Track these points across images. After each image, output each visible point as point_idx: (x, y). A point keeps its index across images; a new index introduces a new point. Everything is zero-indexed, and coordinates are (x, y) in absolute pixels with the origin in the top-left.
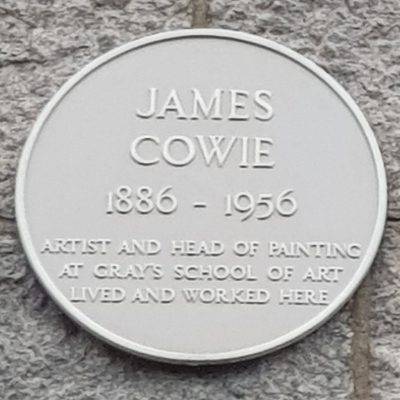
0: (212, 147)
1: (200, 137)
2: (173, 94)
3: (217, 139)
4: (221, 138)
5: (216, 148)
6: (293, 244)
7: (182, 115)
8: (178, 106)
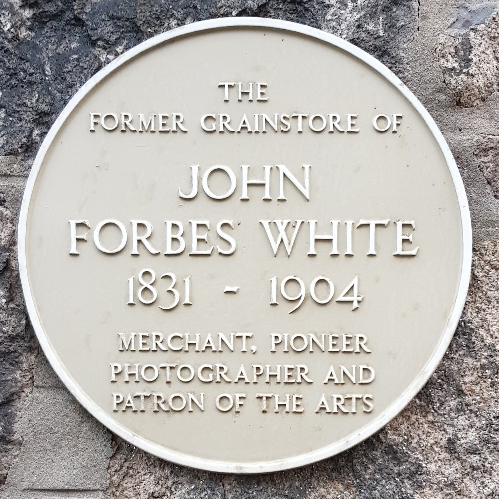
0: (279, 232)
1: (265, 223)
3: (282, 223)
4: (286, 222)
5: (283, 234)
6: (354, 366)
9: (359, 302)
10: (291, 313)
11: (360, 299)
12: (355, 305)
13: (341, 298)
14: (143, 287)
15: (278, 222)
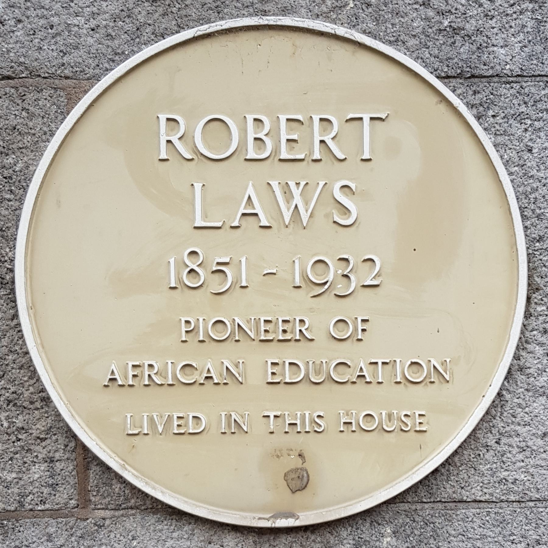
2: (250, 191)
5: (298, 200)
7: (264, 223)
8: (258, 210)
14: (188, 269)
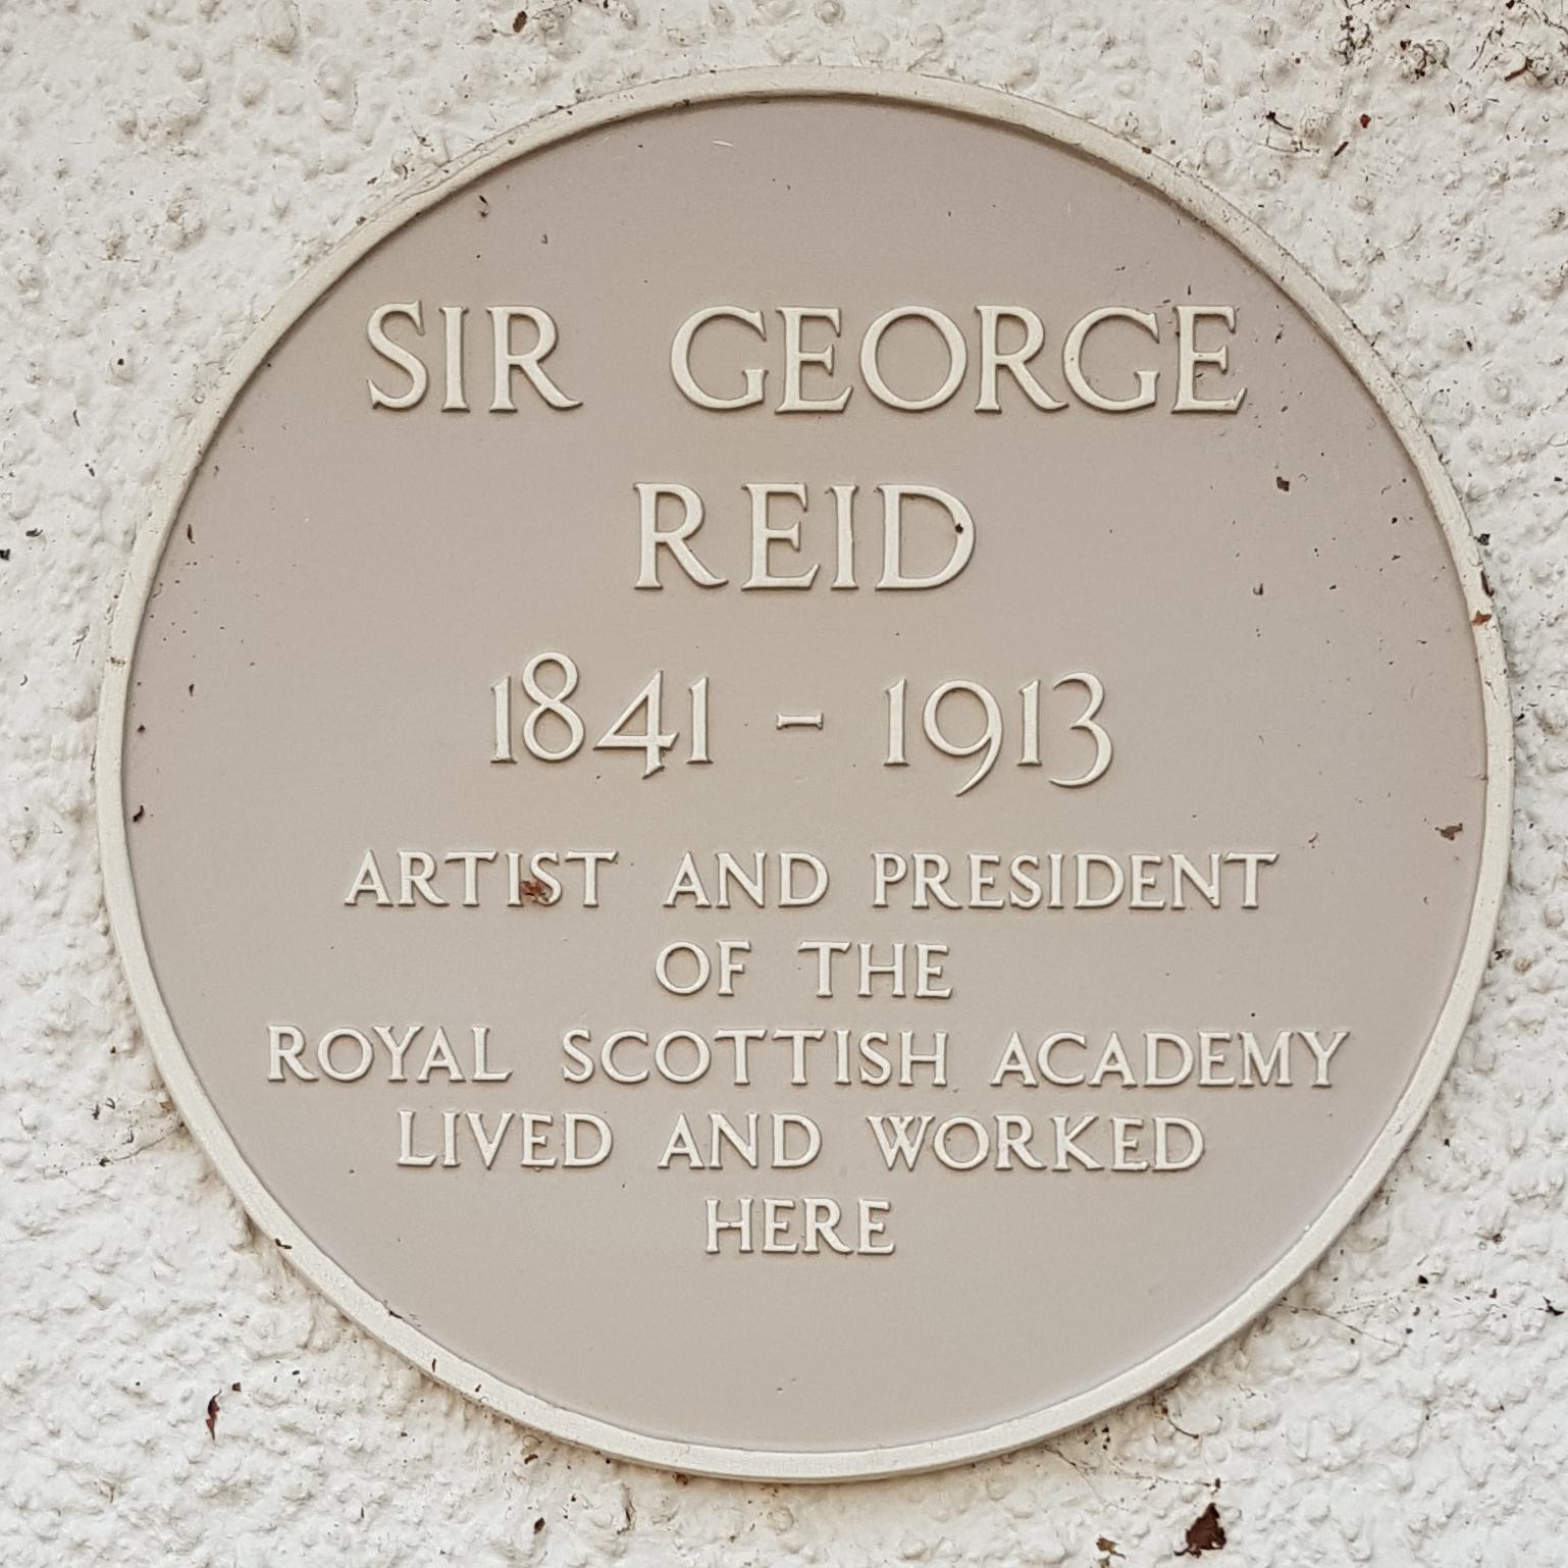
1: (876, 1121)
3: (902, 1120)
4: (908, 1119)
9: (663, 750)
10: (1053, 783)
11: (667, 741)
12: (653, 761)
13: (609, 740)
14: (541, 709)
15: (895, 1120)
